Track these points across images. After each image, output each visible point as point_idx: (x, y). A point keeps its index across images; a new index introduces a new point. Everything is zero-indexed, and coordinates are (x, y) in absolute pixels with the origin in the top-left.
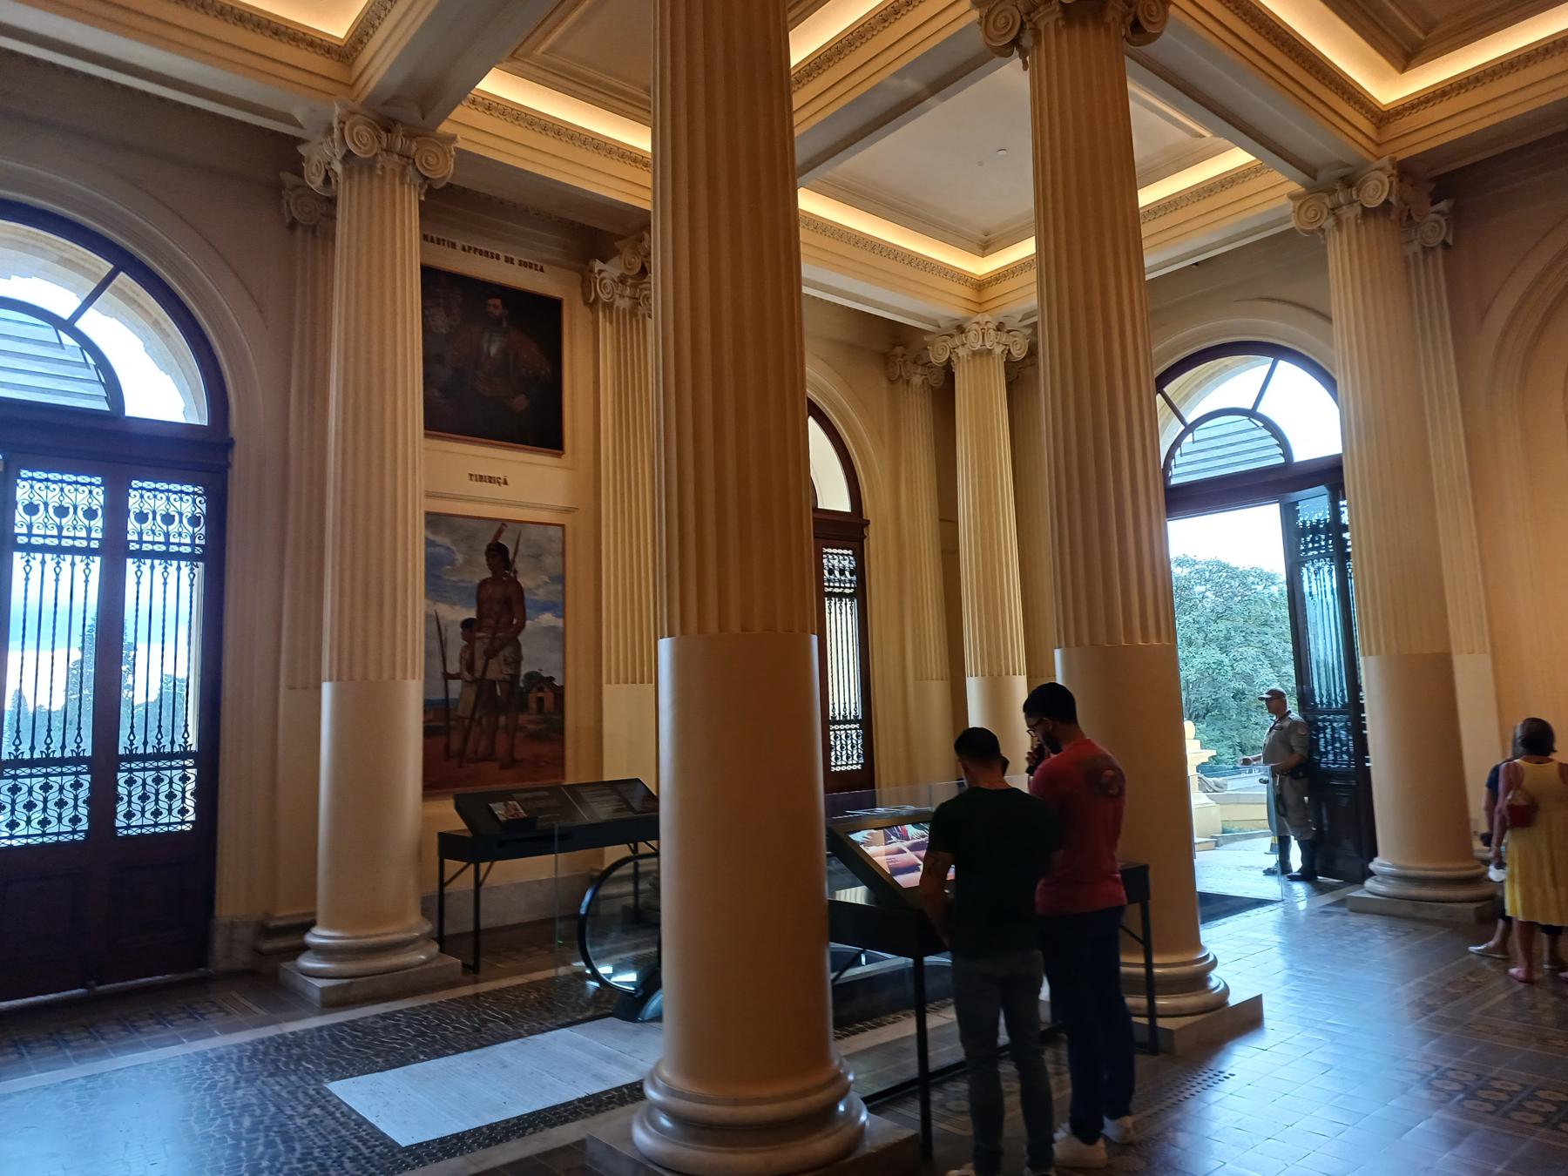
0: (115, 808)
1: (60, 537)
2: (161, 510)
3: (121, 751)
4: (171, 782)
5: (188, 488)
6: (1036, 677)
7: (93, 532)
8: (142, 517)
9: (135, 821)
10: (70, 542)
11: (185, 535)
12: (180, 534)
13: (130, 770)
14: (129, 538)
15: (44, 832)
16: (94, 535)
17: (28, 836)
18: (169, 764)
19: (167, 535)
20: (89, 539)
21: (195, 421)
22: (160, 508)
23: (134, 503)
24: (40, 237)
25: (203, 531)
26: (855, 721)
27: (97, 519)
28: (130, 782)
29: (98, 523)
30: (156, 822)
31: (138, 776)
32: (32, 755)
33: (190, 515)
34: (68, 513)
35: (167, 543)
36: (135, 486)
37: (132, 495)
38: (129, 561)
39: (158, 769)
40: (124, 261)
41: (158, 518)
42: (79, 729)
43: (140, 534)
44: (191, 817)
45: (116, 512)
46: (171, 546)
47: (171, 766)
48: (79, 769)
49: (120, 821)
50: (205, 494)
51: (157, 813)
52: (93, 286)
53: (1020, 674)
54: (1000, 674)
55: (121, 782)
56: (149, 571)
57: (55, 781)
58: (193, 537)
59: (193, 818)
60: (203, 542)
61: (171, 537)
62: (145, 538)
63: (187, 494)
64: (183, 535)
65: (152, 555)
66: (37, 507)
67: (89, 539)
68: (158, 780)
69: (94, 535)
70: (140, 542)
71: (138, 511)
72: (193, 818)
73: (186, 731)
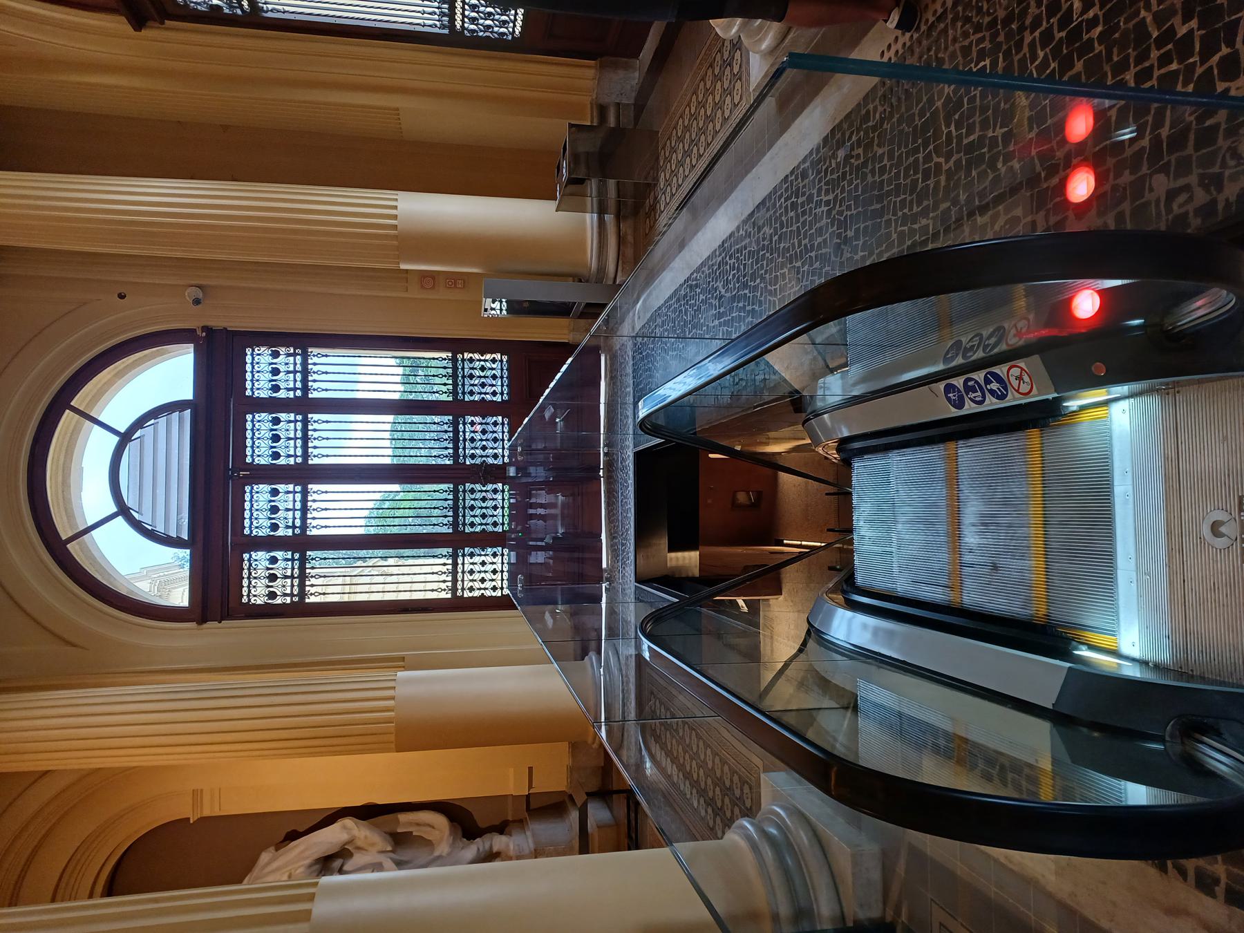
0: (491, 464)
1: (296, 439)
2: (269, 376)
3: (450, 399)
4: (473, 385)
5: (249, 359)
6: (401, 132)
7: (289, 436)
8: (276, 388)
9: (498, 389)
10: (296, 571)
11: (287, 360)
12: (287, 364)
13: (464, 393)
14: (290, 534)
15: (501, 440)
16: (291, 489)
17: (503, 432)
18: (460, 370)
19: (288, 372)
20: (296, 421)
21: (192, 350)
22: (267, 426)
23: (264, 394)
24: (54, 468)
25: (282, 486)
26: (454, 557)
27: (279, 434)
28: (471, 393)
29: (283, 416)
30: (501, 424)
31: (467, 389)
32: (450, 432)
33: (271, 357)
34: (277, 434)
35: (296, 439)
36: (249, 532)
37: (258, 462)
38: (310, 462)
39: (463, 377)
40: (61, 402)
41: (275, 361)
42: (435, 491)
43: (289, 390)
44: (498, 356)
45: (273, 405)
46: (297, 369)
47: (462, 500)
48: (461, 422)
49: (498, 398)
50: (252, 413)
51: (494, 572)
52: (88, 423)
53: (396, 207)
54: (395, 237)
55: (472, 398)
56: (317, 366)
57: (469, 503)
58: (289, 355)
59: (499, 355)
60: (290, 553)
61: (290, 369)
62: (289, 573)
63: (250, 583)
64: (287, 362)
65: (305, 381)
66: (273, 452)
67: (293, 560)
68: (471, 377)
69: (292, 351)
70: (292, 595)
71: (271, 375)
72: (499, 355)
73: (437, 359)
